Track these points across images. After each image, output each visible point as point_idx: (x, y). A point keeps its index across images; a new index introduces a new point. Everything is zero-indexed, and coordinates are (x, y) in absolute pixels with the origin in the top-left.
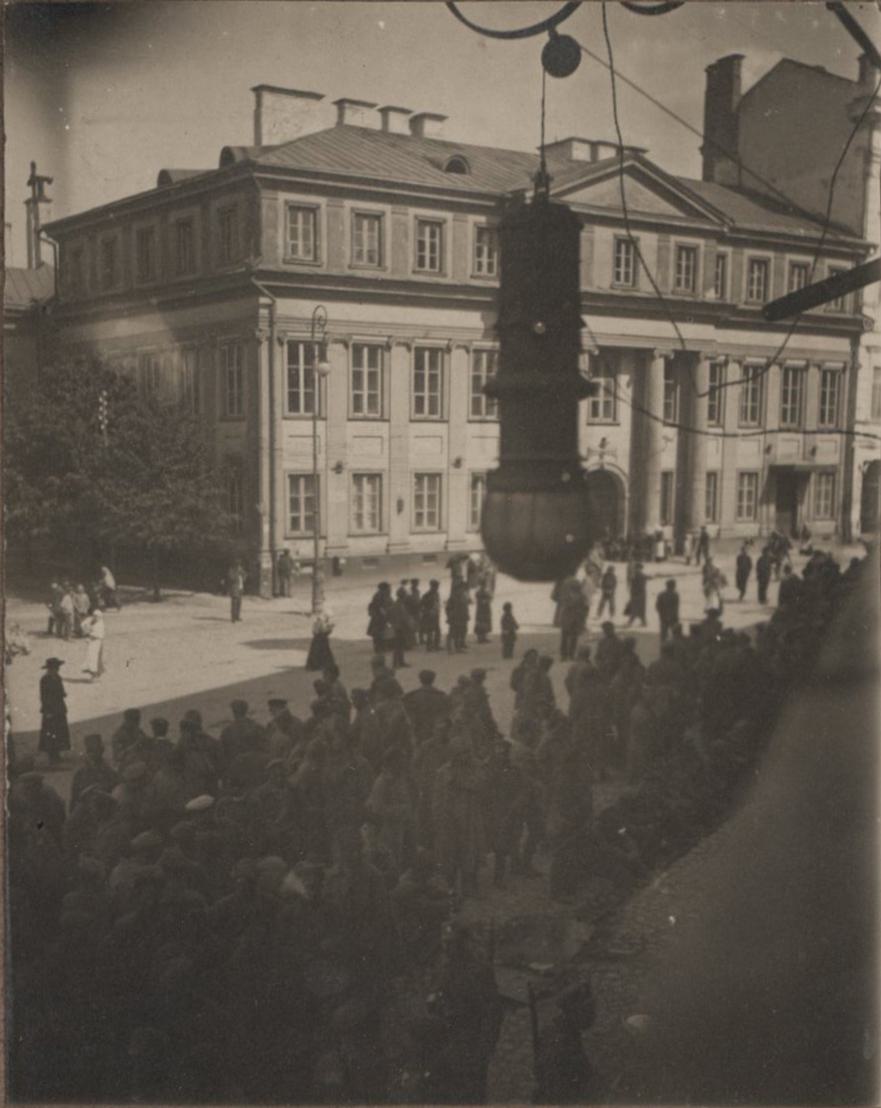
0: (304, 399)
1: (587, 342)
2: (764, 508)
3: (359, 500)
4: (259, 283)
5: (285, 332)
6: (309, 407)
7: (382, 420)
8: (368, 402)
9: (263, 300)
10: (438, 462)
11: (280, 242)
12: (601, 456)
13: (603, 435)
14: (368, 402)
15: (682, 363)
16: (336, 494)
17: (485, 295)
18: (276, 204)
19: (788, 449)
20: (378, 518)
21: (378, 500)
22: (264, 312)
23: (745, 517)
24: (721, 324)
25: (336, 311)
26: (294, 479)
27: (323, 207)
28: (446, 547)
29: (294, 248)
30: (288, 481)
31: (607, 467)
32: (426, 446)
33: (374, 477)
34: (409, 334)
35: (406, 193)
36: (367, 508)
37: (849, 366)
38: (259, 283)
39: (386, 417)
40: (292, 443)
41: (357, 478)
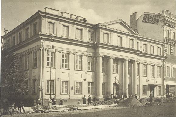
0: (51, 63)
1: (101, 54)
2: (148, 91)
3: (63, 87)
4: (41, 37)
5: (47, 49)
6: (52, 65)
7: (146, 76)
8: (66, 65)
9: (42, 41)
10: (80, 80)
11: (45, 28)
12: (115, 80)
13: (116, 76)
14: (66, 65)
15: (131, 62)
16: (58, 86)
17: (89, 44)
18: (45, 22)
19: (152, 82)
20: (67, 92)
21: (67, 87)
22: (41, 43)
23: (144, 95)
24: (139, 55)
25: (56, 45)
26: (48, 81)
27: (70, 26)
28: (69, 98)
29: (49, 31)
30: (47, 81)
31: (117, 83)
32: (77, 76)
33: (67, 82)
34: (60, 49)
35: (57, 18)
36: (64, 89)
37: (162, 66)
38: (41, 37)
39: (55, 67)
40: (46, 73)
41: (63, 82)
